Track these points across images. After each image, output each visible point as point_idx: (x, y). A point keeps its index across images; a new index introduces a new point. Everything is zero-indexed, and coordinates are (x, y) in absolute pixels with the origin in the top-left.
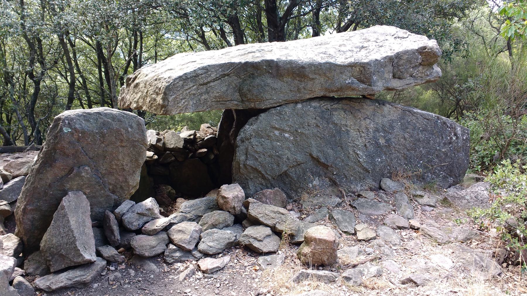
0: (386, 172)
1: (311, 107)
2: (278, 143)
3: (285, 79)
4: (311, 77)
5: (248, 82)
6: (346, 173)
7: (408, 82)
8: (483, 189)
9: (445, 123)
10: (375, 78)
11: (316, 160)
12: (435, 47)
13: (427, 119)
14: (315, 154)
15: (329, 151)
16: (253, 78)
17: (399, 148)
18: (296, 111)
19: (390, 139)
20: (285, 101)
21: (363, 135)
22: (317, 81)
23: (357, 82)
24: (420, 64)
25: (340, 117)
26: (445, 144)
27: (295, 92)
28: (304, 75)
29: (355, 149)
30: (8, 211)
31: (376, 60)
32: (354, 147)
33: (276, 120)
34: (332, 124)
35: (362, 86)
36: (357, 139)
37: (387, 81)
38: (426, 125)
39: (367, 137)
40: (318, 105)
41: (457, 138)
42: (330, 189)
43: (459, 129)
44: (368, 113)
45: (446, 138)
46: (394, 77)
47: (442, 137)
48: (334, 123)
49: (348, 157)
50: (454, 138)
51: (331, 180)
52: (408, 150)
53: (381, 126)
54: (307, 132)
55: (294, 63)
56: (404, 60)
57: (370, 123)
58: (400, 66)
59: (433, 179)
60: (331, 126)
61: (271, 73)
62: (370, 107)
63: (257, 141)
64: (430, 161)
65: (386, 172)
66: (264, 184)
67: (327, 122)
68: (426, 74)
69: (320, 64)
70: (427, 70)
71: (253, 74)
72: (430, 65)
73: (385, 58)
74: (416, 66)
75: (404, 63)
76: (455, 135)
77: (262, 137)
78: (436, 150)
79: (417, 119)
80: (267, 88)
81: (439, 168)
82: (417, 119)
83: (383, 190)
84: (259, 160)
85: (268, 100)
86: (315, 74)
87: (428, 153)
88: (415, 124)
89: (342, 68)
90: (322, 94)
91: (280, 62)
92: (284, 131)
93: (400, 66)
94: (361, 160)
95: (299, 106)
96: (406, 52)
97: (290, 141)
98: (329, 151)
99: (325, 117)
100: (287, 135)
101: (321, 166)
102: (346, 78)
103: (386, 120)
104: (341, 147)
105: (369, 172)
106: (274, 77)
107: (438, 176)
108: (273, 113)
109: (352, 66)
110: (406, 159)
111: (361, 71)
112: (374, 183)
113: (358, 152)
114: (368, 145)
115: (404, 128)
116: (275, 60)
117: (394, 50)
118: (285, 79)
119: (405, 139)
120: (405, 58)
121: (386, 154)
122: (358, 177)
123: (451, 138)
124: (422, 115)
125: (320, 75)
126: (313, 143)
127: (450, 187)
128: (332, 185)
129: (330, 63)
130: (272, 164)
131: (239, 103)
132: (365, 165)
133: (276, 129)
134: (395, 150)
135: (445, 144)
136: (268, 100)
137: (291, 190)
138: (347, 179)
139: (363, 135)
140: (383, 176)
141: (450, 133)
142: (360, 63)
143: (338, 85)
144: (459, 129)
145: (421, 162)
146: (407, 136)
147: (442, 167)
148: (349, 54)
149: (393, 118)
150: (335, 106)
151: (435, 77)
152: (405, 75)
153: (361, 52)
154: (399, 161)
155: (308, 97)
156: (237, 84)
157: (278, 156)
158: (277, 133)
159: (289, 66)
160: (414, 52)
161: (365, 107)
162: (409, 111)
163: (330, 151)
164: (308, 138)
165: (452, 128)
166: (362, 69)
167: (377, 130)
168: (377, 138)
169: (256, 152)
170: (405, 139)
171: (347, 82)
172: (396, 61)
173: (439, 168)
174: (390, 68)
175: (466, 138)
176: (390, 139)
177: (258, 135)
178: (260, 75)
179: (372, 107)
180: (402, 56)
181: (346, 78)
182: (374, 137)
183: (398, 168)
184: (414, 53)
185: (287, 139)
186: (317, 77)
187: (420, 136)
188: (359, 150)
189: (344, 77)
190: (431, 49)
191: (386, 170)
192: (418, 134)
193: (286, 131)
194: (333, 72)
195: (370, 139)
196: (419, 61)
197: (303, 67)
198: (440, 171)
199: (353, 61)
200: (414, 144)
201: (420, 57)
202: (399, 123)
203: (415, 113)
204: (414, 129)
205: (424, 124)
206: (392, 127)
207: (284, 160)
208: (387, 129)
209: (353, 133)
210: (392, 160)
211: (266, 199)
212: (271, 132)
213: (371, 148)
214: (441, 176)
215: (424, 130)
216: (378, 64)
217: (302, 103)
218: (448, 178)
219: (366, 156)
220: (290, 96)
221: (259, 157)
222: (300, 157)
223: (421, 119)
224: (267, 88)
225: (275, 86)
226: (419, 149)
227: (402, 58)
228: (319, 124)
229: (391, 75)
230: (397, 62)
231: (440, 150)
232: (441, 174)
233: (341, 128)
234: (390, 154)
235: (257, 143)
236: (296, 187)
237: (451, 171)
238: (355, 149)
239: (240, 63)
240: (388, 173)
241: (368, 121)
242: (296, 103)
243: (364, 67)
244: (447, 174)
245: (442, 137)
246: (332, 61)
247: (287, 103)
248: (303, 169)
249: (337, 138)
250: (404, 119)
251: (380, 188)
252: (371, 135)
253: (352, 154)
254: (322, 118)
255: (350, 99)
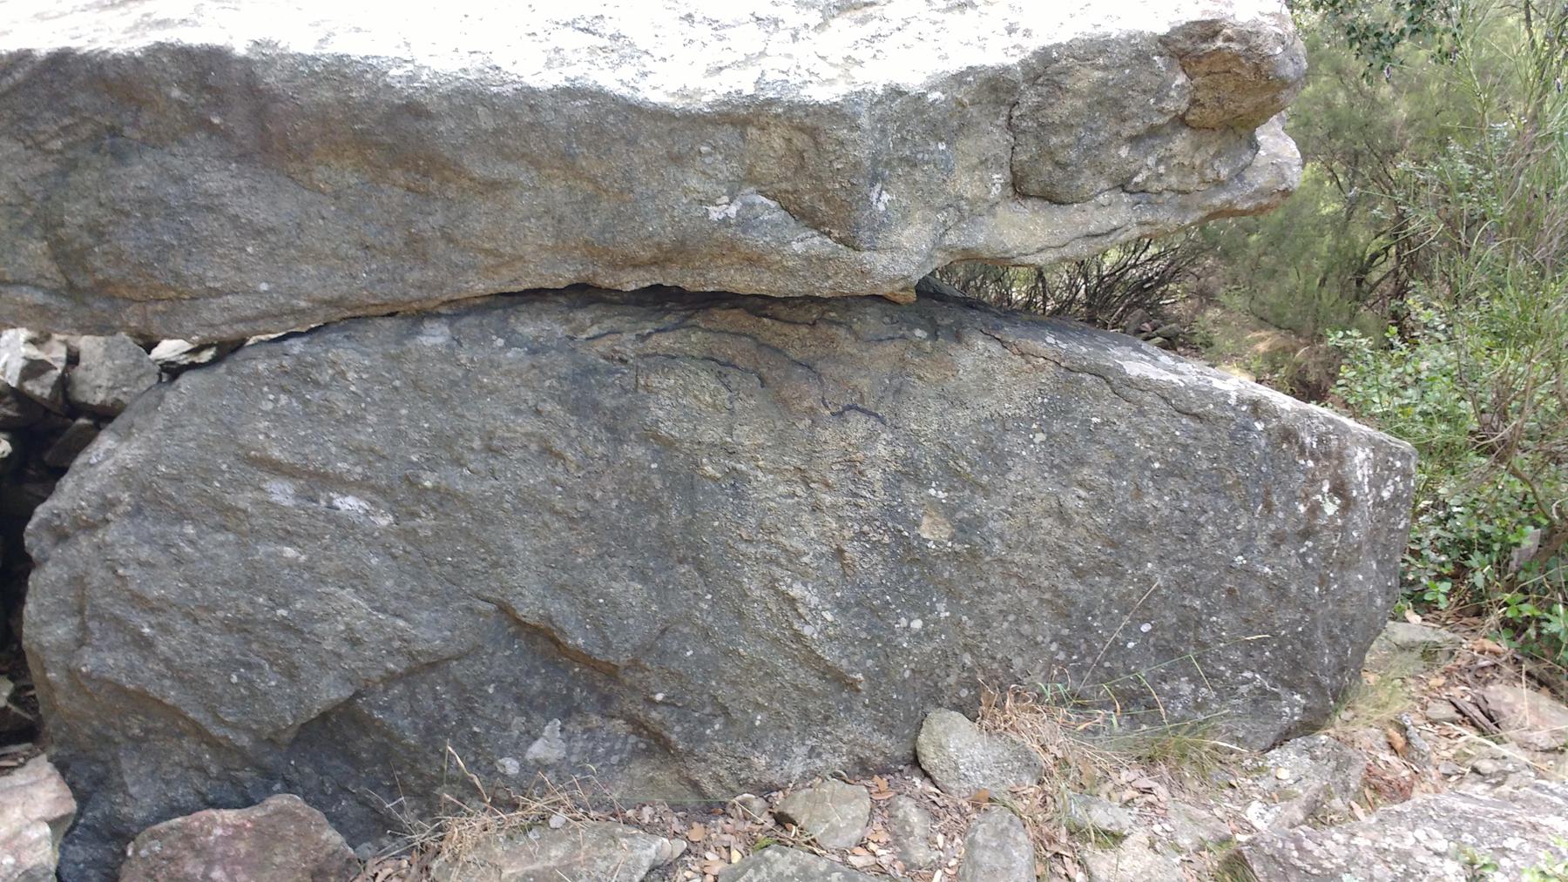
0: (952, 680)
1: (509, 344)
2: (290, 552)
3: (320, 174)
4: (478, 171)
5: (90, 177)
6: (724, 693)
7: (1097, 219)
8: (1441, 846)
9: (1288, 435)
10: (882, 200)
11: (542, 640)
12: (1270, 27)
13: (1197, 416)
14: (528, 609)
15: (616, 588)
16: (119, 156)
17: (1028, 566)
18: (409, 367)
19: (977, 522)
20: (330, 303)
21: (828, 499)
22: (523, 202)
23: (779, 216)
24: (1181, 121)
25: (688, 401)
26: (1277, 539)
27: (396, 255)
28: (430, 160)
29: (778, 572)
30: (13, 418)
31: (896, 92)
32: (773, 561)
33: (277, 417)
34: (643, 439)
35: (805, 243)
36: (793, 521)
37: (967, 211)
38: (1185, 447)
39: (849, 512)
40: (561, 331)
41: (1348, 505)
42: (639, 770)
43: (1361, 455)
44: (864, 384)
45: (1288, 507)
46: (1019, 188)
47: (1269, 506)
48: (657, 438)
49: (740, 615)
50: (1330, 509)
51: (638, 726)
52: (1078, 574)
53: (937, 450)
54: (475, 488)
55: (358, 79)
56: (1077, 94)
57: (872, 437)
58: (1053, 128)
59: (1199, 707)
60: (636, 452)
61: (225, 135)
62: (877, 350)
63: (150, 540)
64: (1191, 622)
65: (952, 680)
66: (214, 770)
67: (609, 429)
68: (1210, 174)
69: (528, 96)
70: (1218, 155)
71: (114, 132)
72: (1238, 130)
73: (959, 79)
74: (1153, 132)
75: (1076, 113)
76: (1340, 489)
77: (182, 516)
78: (1230, 569)
79: (1141, 413)
80: (207, 225)
81: (1236, 656)
82: (1141, 413)
83: (926, 775)
84: (162, 648)
85: (219, 293)
86: (505, 154)
87: (1184, 584)
88: (1125, 440)
89: (681, 131)
90: (566, 275)
91: (269, 63)
92: (317, 481)
93: (1053, 128)
94: (807, 630)
95: (435, 336)
96: (1095, 50)
97: (372, 539)
98: (616, 588)
99: (596, 406)
100: (349, 504)
101: (568, 674)
102: (709, 187)
103: (964, 417)
104: (699, 566)
105: (853, 686)
106: (244, 157)
107: (1227, 692)
108: (257, 376)
109: (740, 119)
110: (1063, 615)
111: (801, 155)
112: (880, 740)
113: (797, 591)
114: (852, 551)
115: (1064, 462)
116: (240, 49)
117: (1027, 33)
118: (320, 174)
119: (1062, 516)
120: (1083, 85)
121: (952, 595)
122: (793, 714)
123: (1315, 509)
124: (1166, 394)
125: (536, 164)
126: (517, 544)
127: (1282, 740)
128: (648, 753)
129: (596, 96)
130: (249, 666)
131: (53, 302)
132: (830, 654)
133: (277, 469)
134: (1008, 575)
135: (1277, 539)
136: (219, 293)
137: (392, 793)
138: (730, 722)
139: (828, 499)
140: (934, 697)
141: (1313, 481)
142: (791, 107)
143: (660, 228)
144: (1361, 455)
145: (1145, 628)
146: (1074, 500)
147: (1249, 649)
148: (747, 39)
149: (1008, 409)
150: (666, 341)
151: (1260, 192)
152: (1086, 180)
153: (830, 32)
154: (1026, 629)
155: (480, 286)
156: (29, 188)
157: (284, 626)
158: (281, 492)
159: (326, 94)
160: (1140, 52)
161: (849, 346)
162: (1100, 374)
163: (629, 592)
164: (484, 520)
165: (1327, 455)
166: (800, 141)
167: (909, 473)
168: (904, 518)
169: (138, 600)
170: (1062, 516)
171: (715, 214)
172: (1030, 98)
173: (1236, 656)
174: (995, 139)
175: (1396, 496)
176: (977, 522)
177: (148, 499)
178: (156, 141)
179: (890, 348)
180: (1066, 71)
181: (709, 187)
182: (890, 511)
183: (1018, 662)
184: (1142, 57)
185: (345, 527)
186: (524, 175)
187: (1150, 500)
188: (802, 576)
189: (693, 182)
190: (1244, 37)
191: (956, 670)
192: (1139, 493)
193: (344, 484)
194: (620, 147)
195: (869, 520)
196: (1169, 105)
197: (413, 109)
198: (1237, 668)
199: (749, 90)
200: (1113, 544)
201: (1181, 79)
202: (1040, 437)
203: (1130, 383)
204: (1118, 467)
205: (1174, 441)
206: (998, 460)
207: (328, 645)
208: (972, 468)
209: (770, 489)
210: (985, 622)
211: (210, 864)
212: (239, 485)
213: (873, 568)
214: (1244, 689)
215: (1173, 470)
216: (902, 121)
217: (452, 318)
218: (1277, 697)
219: (841, 607)
220: (363, 281)
221: (164, 629)
222: (429, 631)
223: (1158, 418)
224: (207, 225)
225: (261, 214)
226: (1138, 565)
227: (1068, 82)
228: (559, 444)
229: (998, 178)
230: (1039, 108)
231: (1248, 571)
232: (1247, 681)
233: (698, 465)
234: (979, 592)
235: (145, 553)
236: (421, 776)
237: (1297, 667)
238: (778, 572)
239: (23, 57)
240: (961, 684)
241: (858, 426)
242: (420, 316)
243: (813, 132)
244: (1277, 680)
245: (1269, 506)
246: (610, 80)
247: (347, 319)
248: (459, 687)
249: (673, 521)
250: (1065, 413)
251: (915, 761)
252: (875, 498)
253: (762, 600)
254: (582, 408)
255: (758, 305)
